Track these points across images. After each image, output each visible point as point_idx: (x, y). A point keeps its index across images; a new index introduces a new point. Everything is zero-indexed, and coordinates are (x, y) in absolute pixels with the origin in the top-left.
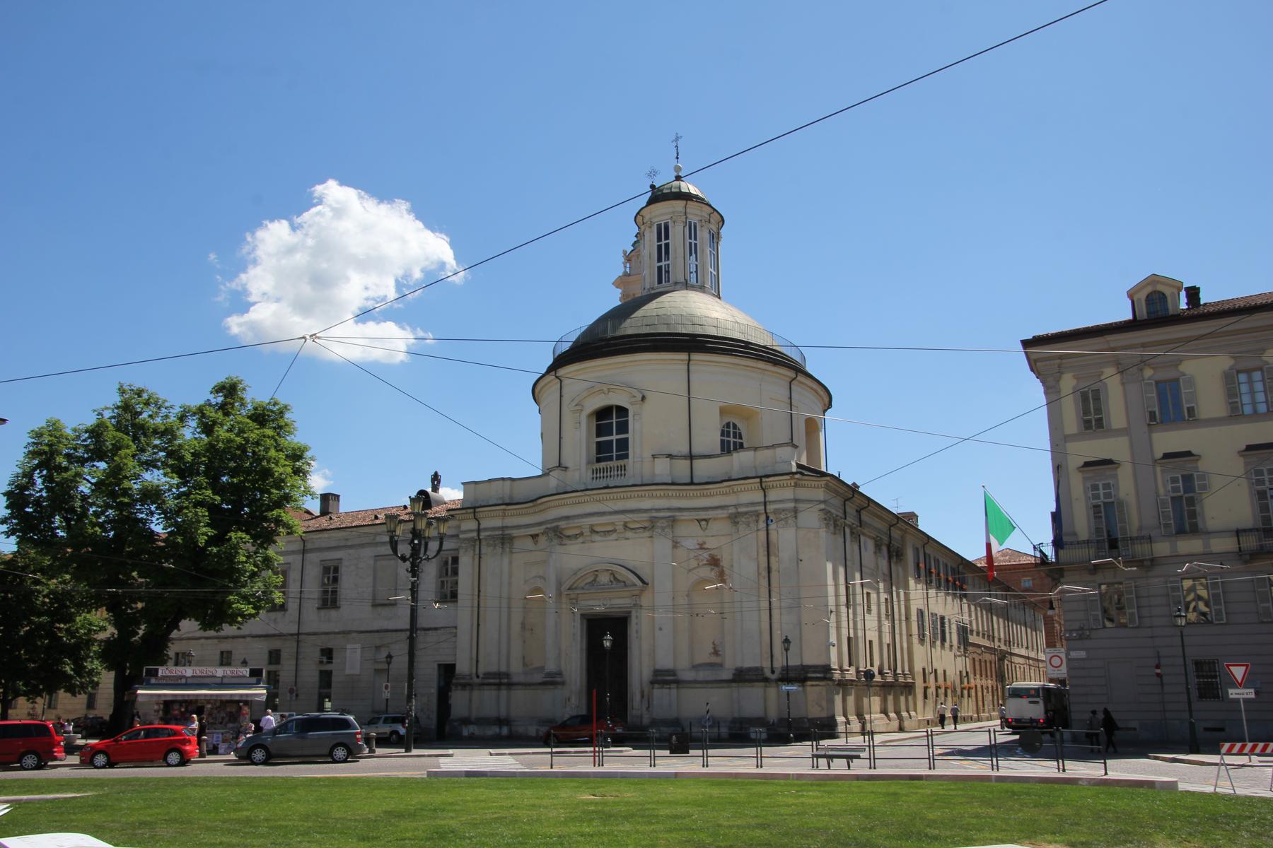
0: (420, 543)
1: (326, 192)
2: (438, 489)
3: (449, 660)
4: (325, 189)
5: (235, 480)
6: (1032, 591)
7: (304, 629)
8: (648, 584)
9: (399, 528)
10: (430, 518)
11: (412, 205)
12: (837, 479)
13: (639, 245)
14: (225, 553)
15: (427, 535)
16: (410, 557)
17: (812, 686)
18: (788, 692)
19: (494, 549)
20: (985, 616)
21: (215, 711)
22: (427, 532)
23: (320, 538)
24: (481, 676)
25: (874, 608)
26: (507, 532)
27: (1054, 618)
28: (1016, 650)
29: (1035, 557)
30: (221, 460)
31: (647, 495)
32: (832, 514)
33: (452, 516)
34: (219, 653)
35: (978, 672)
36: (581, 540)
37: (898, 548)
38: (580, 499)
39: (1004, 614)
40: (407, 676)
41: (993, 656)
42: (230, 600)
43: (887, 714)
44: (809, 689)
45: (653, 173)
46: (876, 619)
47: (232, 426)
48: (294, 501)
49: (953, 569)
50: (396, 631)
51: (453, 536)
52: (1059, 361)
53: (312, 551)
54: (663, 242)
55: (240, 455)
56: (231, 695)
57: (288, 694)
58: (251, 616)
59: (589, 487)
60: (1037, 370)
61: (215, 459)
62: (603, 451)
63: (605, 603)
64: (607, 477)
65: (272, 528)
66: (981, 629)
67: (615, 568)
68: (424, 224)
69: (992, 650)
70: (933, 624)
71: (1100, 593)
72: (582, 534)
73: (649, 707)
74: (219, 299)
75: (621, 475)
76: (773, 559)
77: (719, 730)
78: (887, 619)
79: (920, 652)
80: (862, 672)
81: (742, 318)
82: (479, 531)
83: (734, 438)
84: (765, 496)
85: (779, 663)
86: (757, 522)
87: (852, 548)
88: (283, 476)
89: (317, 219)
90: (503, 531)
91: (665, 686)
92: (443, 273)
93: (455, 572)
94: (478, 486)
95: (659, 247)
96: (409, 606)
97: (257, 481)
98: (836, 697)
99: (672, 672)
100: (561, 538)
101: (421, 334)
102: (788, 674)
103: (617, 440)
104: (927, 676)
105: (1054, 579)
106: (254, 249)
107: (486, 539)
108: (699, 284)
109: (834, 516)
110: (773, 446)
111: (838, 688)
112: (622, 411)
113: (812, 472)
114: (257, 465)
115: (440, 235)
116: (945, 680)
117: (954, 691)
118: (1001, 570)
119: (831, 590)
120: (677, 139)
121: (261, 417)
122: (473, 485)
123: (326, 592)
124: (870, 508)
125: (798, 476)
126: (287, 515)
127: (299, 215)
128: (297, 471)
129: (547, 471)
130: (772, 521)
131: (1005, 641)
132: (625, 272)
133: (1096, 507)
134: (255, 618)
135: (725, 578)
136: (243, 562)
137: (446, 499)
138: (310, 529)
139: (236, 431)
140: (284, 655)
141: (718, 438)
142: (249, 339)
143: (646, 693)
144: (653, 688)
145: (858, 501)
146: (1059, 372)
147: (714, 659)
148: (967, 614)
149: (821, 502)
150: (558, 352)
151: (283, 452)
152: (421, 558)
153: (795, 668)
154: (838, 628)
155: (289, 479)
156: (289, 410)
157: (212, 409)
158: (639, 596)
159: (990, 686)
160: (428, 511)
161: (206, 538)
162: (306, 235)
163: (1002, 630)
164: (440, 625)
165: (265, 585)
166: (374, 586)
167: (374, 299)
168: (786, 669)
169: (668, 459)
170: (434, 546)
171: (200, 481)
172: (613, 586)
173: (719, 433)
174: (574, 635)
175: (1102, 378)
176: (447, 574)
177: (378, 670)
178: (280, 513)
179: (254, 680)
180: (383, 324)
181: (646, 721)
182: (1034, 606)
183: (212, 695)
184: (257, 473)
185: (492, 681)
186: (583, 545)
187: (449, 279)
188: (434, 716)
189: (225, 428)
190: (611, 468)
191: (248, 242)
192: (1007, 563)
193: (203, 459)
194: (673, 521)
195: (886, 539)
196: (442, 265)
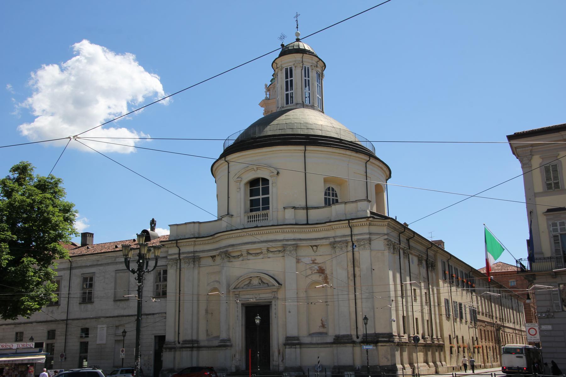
0: (143, 262)
1: (81, 47)
2: (155, 229)
3: (161, 333)
4: (81, 45)
5: (26, 225)
6: (515, 288)
7: (71, 317)
8: (282, 285)
9: (130, 253)
10: (149, 247)
11: (136, 56)
12: (395, 221)
13: (275, 81)
14: (19, 270)
15: (148, 257)
16: (137, 271)
17: (382, 346)
18: (367, 349)
20: (487, 303)
21: (11, 371)
22: (148, 255)
23: (81, 260)
24: (181, 342)
25: (418, 298)
26: (196, 255)
27: (531, 305)
28: (507, 324)
29: (517, 267)
30: (17, 213)
31: (281, 231)
32: (392, 242)
33: (163, 245)
34: (14, 333)
35: (483, 337)
36: (241, 258)
37: (432, 261)
38: (240, 234)
39: (499, 302)
40: (135, 344)
41: (493, 328)
42: (23, 300)
43: (427, 363)
44: (380, 348)
45: (283, 37)
46: (420, 305)
47: (24, 192)
48: (64, 238)
49: (466, 275)
50: (129, 316)
51: (163, 257)
52: (531, 148)
53: (76, 268)
54: (289, 79)
55: (29, 210)
56: (22, 360)
57: (60, 358)
58: (36, 309)
59: (246, 227)
60: (517, 154)
61: (14, 212)
62: (254, 205)
63: (256, 297)
65: (50, 254)
66: (484, 311)
68: (144, 68)
69: (492, 324)
70: (455, 307)
71: (560, 290)
72: (242, 255)
73: (283, 360)
74: (14, 113)
75: (265, 219)
76: (356, 269)
77: (326, 373)
78: (426, 304)
79: (447, 325)
80: (412, 337)
81: (337, 125)
82: (179, 254)
83: (330, 198)
84: (351, 231)
85: (361, 332)
86: (347, 247)
87: (405, 262)
88: (58, 223)
89: (77, 64)
90: (194, 254)
91: (293, 347)
92: (156, 98)
93: (165, 279)
94: (179, 227)
95: (287, 82)
96: (137, 301)
97: (41, 226)
98: (396, 352)
99: (297, 338)
100: (229, 257)
101: (143, 135)
102: (366, 338)
103: (262, 198)
104: (452, 340)
105: (529, 281)
106: (37, 82)
107: (184, 259)
108: (311, 104)
109: (393, 242)
110: (356, 201)
111: (397, 347)
112: (265, 181)
113: (380, 216)
114: (41, 216)
115: (154, 75)
116: (463, 342)
117: (469, 349)
118: (496, 275)
119: (392, 287)
120: (297, 16)
121: (43, 186)
122: (176, 227)
123: (85, 293)
124: (414, 238)
125: (371, 219)
126: (60, 246)
127: (64, 62)
128: (66, 219)
129: (221, 218)
130: (356, 246)
131: (500, 319)
132: (266, 97)
133: (555, 236)
134: (39, 310)
135: (328, 280)
136: (31, 276)
137: (160, 235)
138: (75, 255)
139: (27, 195)
140: (57, 333)
141: (323, 196)
142: (35, 138)
143: (281, 351)
144: (285, 348)
145: (407, 233)
146: (531, 155)
147: (322, 330)
148: (476, 302)
149: (385, 234)
150: (227, 146)
151: (57, 208)
152: (144, 271)
153: (371, 335)
154: (397, 310)
155: (61, 224)
156: (61, 182)
157: (11, 182)
158: (276, 292)
159: (491, 347)
160: (148, 243)
161: (7, 261)
162: (70, 74)
163: (494, 309)
164: (156, 312)
165: (46, 290)
166: (115, 289)
167: (114, 114)
168: (366, 335)
169: (293, 209)
170: (152, 264)
171: (3, 226)
173: (323, 194)
174: (237, 316)
175: (558, 157)
176: (160, 281)
177: (117, 340)
178: (56, 245)
179: (37, 350)
180: (120, 129)
181: (281, 368)
182: (517, 297)
183: (9, 361)
184: (40, 221)
185: (187, 345)
186: (242, 262)
187: (160, 102)
188: (152, 368)
189: (20, 193)
190: (259, 215)
191: (32, 78)
192: (499, 271)
193: (5, 213)
194: (296, 247)
195: (425, 256)
196: (156, 94)
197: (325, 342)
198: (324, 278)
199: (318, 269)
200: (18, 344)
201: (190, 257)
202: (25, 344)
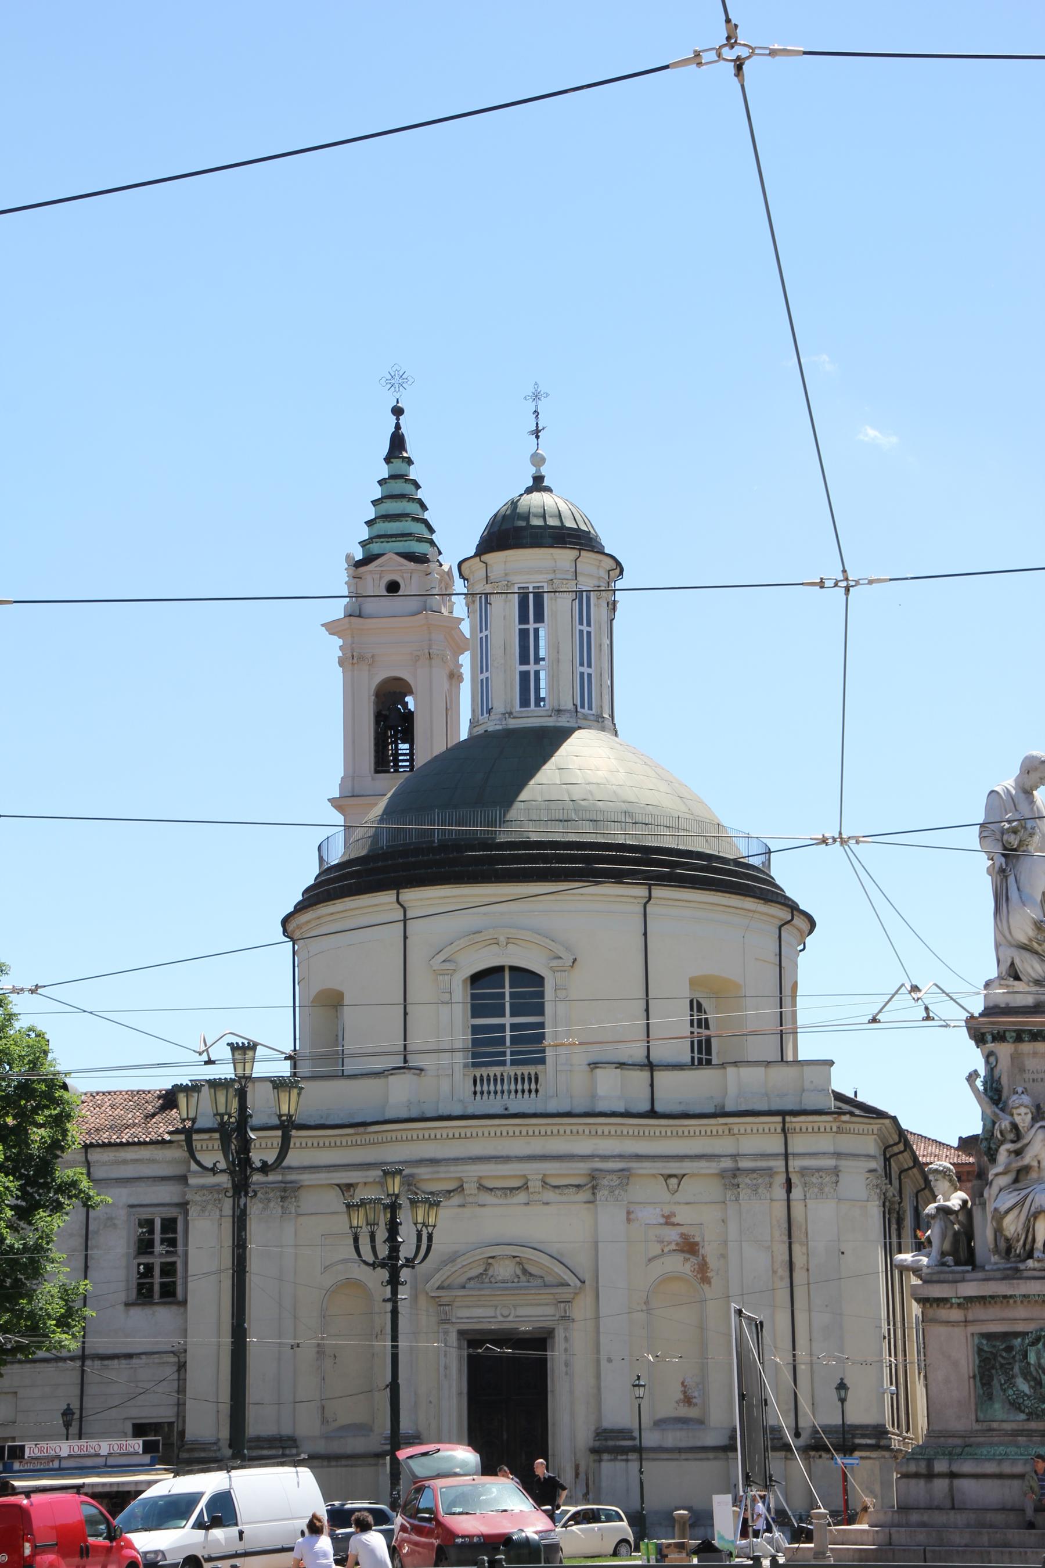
19: (264, 1209)
44: (604, 1464)
63: (505, 1313)
64: (503, 1092)
67: (528, 1253)
76: (796, 1248)
91: (619, 1457)
108: (594, 712)
120: (536, 396)
135: (708, 1274)
143: (582, 1469)
144: (600, 1461)
147: (684, 1411)
172: (520, 1284)
179: (147, 1459)
186: (460, 1210)
194: (625, 1176)
197: (699, 1444)
198: (696, 1266)
199: (679, 1240)
200: (110, 1443)
201: (269, 1183)
202: (124, 1443)
